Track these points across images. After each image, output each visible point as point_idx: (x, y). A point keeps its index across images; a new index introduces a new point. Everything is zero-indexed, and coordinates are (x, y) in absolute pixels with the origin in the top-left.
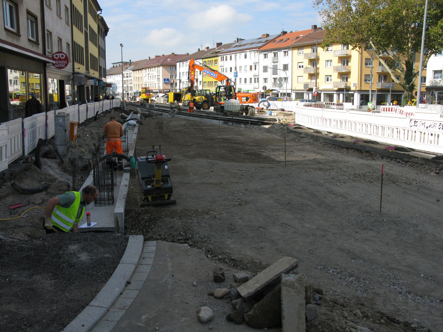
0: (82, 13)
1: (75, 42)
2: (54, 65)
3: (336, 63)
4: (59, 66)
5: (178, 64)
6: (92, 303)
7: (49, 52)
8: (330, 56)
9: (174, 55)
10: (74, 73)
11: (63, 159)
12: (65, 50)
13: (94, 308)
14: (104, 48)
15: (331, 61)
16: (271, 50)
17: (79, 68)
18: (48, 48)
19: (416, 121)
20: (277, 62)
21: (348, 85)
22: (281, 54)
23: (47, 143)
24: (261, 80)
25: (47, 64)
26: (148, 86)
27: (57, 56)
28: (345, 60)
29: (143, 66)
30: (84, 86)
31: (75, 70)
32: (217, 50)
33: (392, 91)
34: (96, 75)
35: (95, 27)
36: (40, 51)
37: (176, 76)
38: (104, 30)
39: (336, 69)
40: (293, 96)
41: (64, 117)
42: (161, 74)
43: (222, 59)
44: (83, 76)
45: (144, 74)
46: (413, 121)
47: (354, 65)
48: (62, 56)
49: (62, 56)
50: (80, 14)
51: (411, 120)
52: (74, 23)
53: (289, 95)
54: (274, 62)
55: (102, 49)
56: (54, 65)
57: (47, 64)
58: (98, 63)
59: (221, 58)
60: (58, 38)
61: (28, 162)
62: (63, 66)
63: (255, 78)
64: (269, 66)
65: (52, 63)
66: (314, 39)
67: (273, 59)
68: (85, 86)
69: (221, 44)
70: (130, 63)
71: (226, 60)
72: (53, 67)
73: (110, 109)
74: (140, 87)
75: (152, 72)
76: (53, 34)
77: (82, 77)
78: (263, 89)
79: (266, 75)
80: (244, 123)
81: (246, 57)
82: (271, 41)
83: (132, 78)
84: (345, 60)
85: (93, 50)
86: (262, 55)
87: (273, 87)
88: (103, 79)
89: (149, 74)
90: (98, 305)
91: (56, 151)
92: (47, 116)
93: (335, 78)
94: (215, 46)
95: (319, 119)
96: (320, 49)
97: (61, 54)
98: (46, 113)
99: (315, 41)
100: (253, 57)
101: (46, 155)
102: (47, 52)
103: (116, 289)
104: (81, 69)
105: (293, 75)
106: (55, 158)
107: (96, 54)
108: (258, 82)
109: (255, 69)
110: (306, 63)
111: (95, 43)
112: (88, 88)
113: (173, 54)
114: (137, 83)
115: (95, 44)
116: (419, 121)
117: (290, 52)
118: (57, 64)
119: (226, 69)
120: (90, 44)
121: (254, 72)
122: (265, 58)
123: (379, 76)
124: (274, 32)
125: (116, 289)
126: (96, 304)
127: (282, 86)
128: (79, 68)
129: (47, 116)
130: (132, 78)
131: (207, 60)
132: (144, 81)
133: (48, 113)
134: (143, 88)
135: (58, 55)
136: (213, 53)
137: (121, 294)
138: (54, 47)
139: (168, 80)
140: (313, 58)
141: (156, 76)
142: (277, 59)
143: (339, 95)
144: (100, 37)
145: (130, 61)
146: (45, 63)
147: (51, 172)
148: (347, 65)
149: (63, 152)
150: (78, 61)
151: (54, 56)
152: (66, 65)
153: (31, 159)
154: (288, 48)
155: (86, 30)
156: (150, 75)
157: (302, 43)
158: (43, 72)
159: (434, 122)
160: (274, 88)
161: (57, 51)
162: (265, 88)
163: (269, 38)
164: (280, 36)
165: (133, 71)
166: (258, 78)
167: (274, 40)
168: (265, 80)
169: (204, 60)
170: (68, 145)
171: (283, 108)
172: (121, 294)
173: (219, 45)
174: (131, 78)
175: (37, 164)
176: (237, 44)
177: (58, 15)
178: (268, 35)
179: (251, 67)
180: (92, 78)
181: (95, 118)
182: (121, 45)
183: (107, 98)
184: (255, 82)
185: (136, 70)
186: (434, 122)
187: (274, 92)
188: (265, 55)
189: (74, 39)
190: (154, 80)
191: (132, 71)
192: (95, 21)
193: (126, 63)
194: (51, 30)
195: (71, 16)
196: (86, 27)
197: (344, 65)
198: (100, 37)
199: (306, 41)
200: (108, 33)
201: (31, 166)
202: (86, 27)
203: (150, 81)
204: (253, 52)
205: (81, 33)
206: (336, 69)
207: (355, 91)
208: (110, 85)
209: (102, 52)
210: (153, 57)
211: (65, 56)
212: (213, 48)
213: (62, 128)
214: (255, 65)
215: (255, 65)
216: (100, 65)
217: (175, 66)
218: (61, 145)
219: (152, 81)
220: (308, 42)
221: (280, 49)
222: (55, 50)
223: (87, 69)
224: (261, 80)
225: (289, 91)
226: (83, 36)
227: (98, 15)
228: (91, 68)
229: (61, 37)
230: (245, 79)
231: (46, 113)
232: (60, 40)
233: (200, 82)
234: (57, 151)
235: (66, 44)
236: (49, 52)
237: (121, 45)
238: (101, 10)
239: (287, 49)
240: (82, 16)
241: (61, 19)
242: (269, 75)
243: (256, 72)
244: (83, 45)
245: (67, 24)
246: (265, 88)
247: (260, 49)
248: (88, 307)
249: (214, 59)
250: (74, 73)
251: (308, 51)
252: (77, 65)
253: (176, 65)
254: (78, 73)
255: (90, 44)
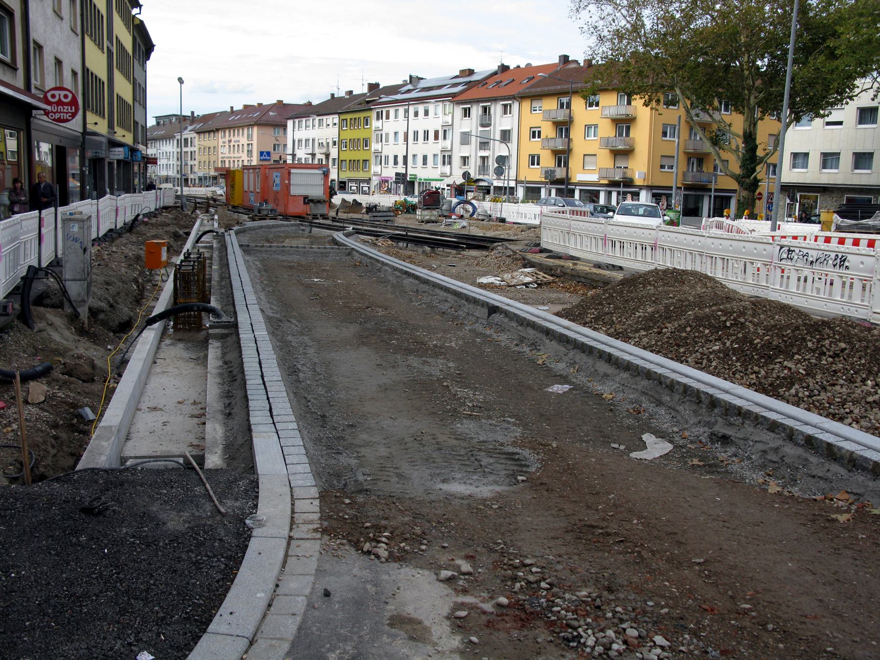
0: (103, 11)
1: (88, 70)
2: (47, 113)
3: (607, 130)
4: (57, 116)
5: (290, 123)
6: (212, 627)
7: (36, 88)
8: (593, 118)
9: (280, 106)
10: (85, 132)
11: (79, 310)
12: (68, 82)
13: (219, 637)
14: (143, 85)
15: (596, 126)
16: (478, 101)
17: (96, 124)
18: (36, 80)
19: (792, 249)
20: (489, 125)
21: (629, 175)
22: (497, 109)
23: (41, 274)
24: (456, 161)
25: (34, 112)
26: (227, 166)
27: (53, 96)
28: (624, 124)
29: (218, 126)
30: (103, 159)
31: (88, 126)
32: (368, 97)
33: (716, 190)
34: (128, 139)
35: (127, 41)
36: (20, 83)
37: (285, 145)
38: (145, 45)
39: (606, 142)
40: (520, 193)
41: (83, 221)
42: (255, 142)
43: (379, 117)
44: (104, 140)
45: (221, 141)
46: (786, 249)
47: (642, 135)
48: (66, 96)
49: (66, 96)
50: (99, 11)
51: (781, 248)
52: (87, 30)
53: (512, 190)
54: (482, 126)
55: (140, 85)
56: (47, 113)
57: (34, 112)
58: (129, 112)
59: (378, 113)
60: (56, 59)
61: (8, 315)
62: (67, 116)
63: (444, 156)
64: (474, 133)
65: (44, 110)
66: (563, 82)
67: (482, 119)
68: (107, 160)
69: (377, 85)
70: (193, 119)
71: (388, 118)
72: (45, 118)
73: (156, 209)
74: (212, 167)
75: (236, 138)
76: (46, 50)
77: (101, 142)
78: (464, 178)
79: (465, 151)
80: (432, 243)
81: (426, 113)
82: (477, 82)
83: (196, 149)
84: (624, 124)
85: (123, 88)
86: (459, 111)
87: (479, 174)
88: (141, 147)
89: (230, 141)
90: (227, 632)
91: (64, 292)
92: (40, 219)
93: (605, 160)
94: (365, 90)
95: (600, 241)
96: (578, 104)
97: (63, 93)
98: (40, 213)
99: (566, 87)
100: (438, 115)
101: (40, 300)
102: (33, 87)
103: (259, 595)
104: (99, 125)
105: (522, 152)
106: (61, 306)
107: (128, 97)
108: (450, 163)
109: (445, 138)
110: (548, 130)
111: (128, 75)
112: (111, 164)
113: (280, 102)
114: (206, 158)
115: (127, 75)
116: (797, 250)
117: (516, 106)
118: (55, 113)
119: (387, 135)
120: (118, 76)
121: (442, 143)
122: (505, 113)
123: (689, 159)
124: (485, 66)
125: (259, 595)
126: (224, 629)
127: (502, 174)
128: (96, 124)
129: (40, 219)
130: (196, 149)
131: (348, 117)
132: (220, 155)
133: (44, 212)
134: (216, 169)
135: (56, 93)
136: (361, 104)
137: (270, 605)
138: (46, 76)
139: (269, 154)
140: (560, 119)
141: (246, 146)
142: (490, 119)
143: (609, 193)
144: (136, 62)
145: (193, 113)
146: (26, 110)
147: (56, 337)
148: (628, 134)
149: (79, 295)
150: (93, 109)
151: (49, 95)
152: (74, 115)
153: (13, 309)
154: (513, 98)
155: (110, 45)
156: (232, 144)
157: (539, 89)
158: (24, 127)
159: (826, 253)
160: (481, 177)
161: (53, 86)
162: (466, 175)
163: (474, 78)
164: (495, 73)
165: (198, 133)
166: (450, 157)
167: (484, 82)
168: (465, 160)
169: (343, 117)
170: (89, 279)
171: (504, 216)
172: (270, 605)
173: (373, 87)
174: (193, 149)
175: (25, 317)
176: (410, 87)
177: (55, 11)
178: (471, 72)
179: (436, 134)
180: (121, 145)
181: (131, 227)
182: (181, 80)
183: (151, 187)
184: (444, 163)
185: (204, 132)
186: (826, 253)
187: (482, 184)
188: (505, 106)
189: (87, 64)
190: (241, 154)
191: (195, 135)
192: (128, 28)
193: (185, 118)
194: (41, 42)
195: (82, 15)
196: (110, 38)
197: (621, 135)
198: (136, 62)
199: (546, 85)
200: (153, 55)
201: (13, 321)
202: (110, 38)
203: (232, 155)
204: (441, 104)
205: (100, 52)
206: (606, 142)
207: (641, 188)
208: (154, 161)
209: (140, 91)
210: (238, 107)
211: (70, 96)
212: (360, 92)
213: (78, 245)
214: (445, 131)
215: (445, 131)
216: (136, 119)
217: (285, 127)
218: (74, 280)
219: (236, 155)
220: (552, 88)
221: (495, 100)
222: (50, 83)
223: (111, 126)
224: (456, 161)
225: (512, 184)
226: (104, 58)
227: (134, 16)
228: (119, 125)
229: (60, 57)
230: (425, 158)
231: (40, 213)
232: (59, 62)
233: (334, 159)
234: (66, 291)
235: (70, 74)
236: (36, 88)
237: (181, 80)
238: (140, 6)
239: (508, 99)
240: (102, 17)
241: (62, 19)
242: (471, 151)
243: (447, 144)
244: (103, 75)
245: (73, 30)
246: (466, 175)
247: (455, 99)
248: (205, 637)
249: (362, 115)
250: (85, 132)
251: (551, 104)
252: (91, 118)
253: (286, 126)
254: (95, 134)
255: (118, 76)
